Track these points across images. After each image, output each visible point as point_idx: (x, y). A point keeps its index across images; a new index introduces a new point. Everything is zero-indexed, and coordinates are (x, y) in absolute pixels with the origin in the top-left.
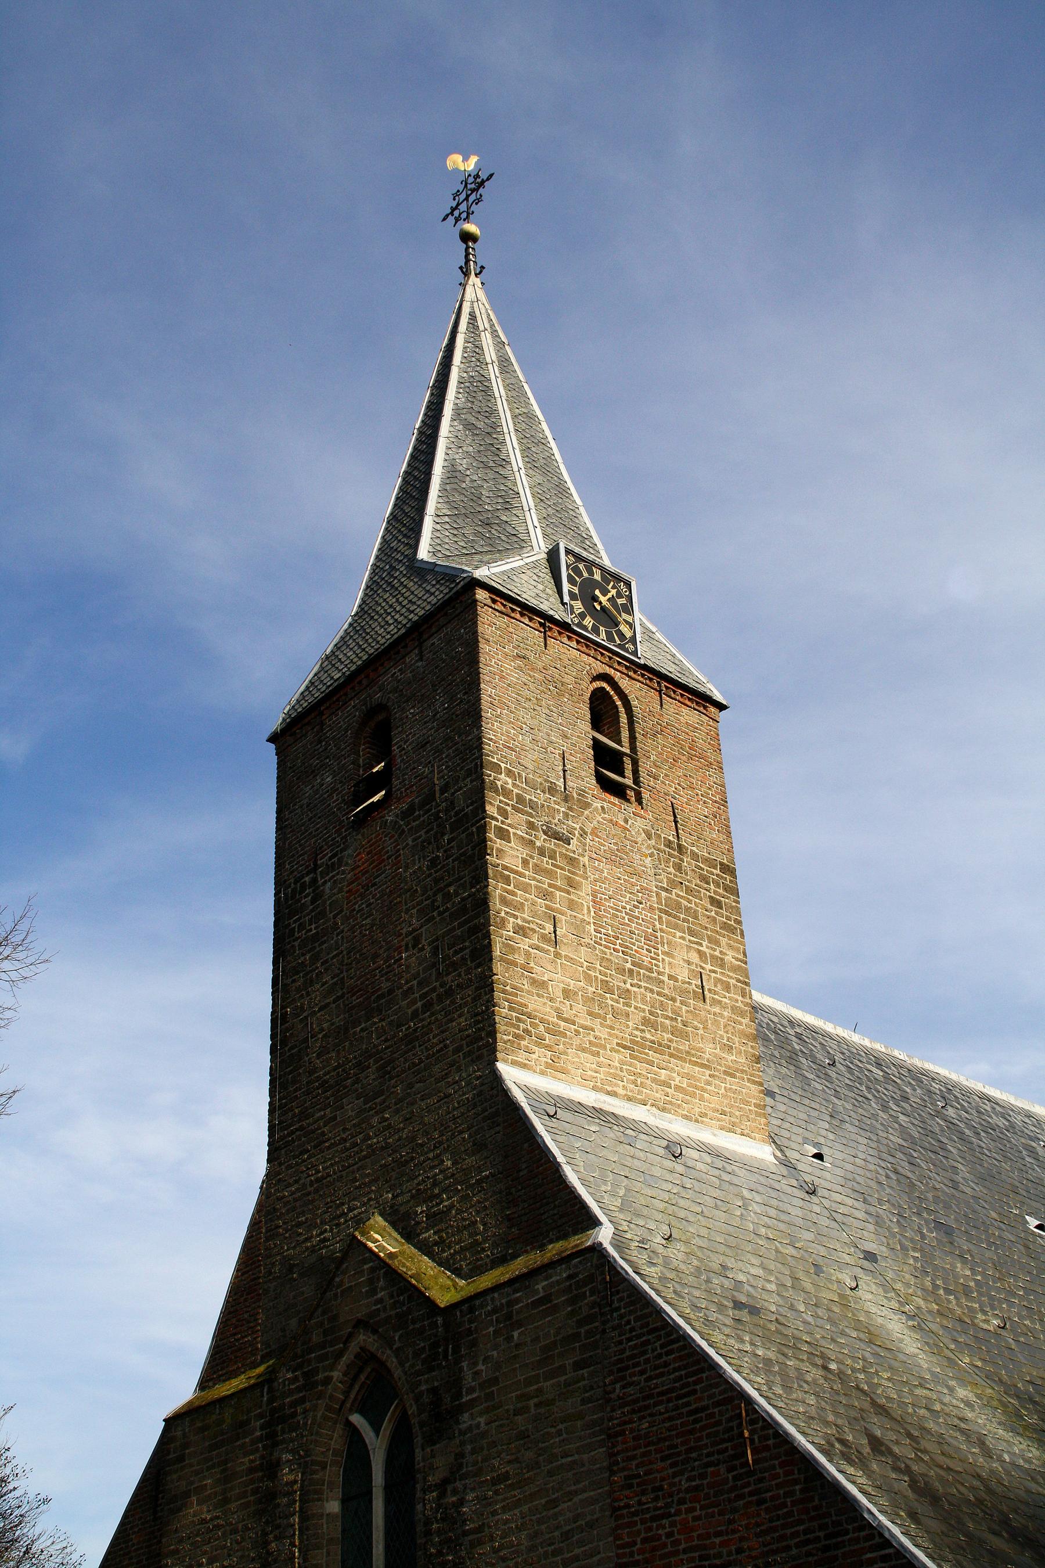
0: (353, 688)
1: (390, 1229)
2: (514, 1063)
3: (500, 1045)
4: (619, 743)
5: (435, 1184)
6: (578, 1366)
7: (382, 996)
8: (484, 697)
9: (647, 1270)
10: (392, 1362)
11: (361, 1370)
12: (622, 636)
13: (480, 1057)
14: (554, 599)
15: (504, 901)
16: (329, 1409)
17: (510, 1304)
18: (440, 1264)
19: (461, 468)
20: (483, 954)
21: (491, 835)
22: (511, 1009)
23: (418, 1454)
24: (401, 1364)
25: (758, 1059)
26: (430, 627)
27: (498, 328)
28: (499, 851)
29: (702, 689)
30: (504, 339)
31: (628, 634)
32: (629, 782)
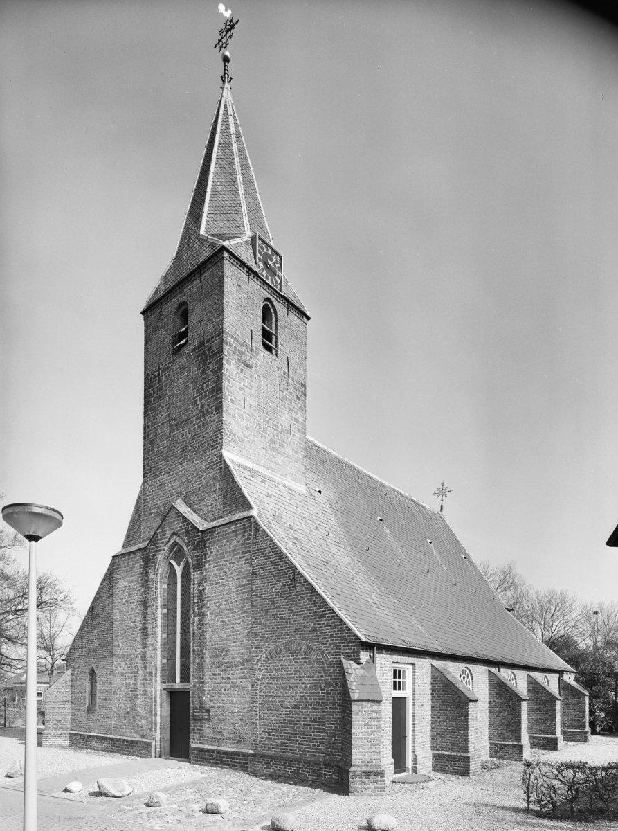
0: (174, 294)
4: (271, 329)
6: (243, 553)
10: (184, 546)
12: (276, 282)
19: (218, 190)
25: (305, 457)
26: (205, 268)
27: (236, 115)
28: (227, 369)
29: (303, 309)
30: (239, 124)
31: (279, 281)
32: (273, 346)
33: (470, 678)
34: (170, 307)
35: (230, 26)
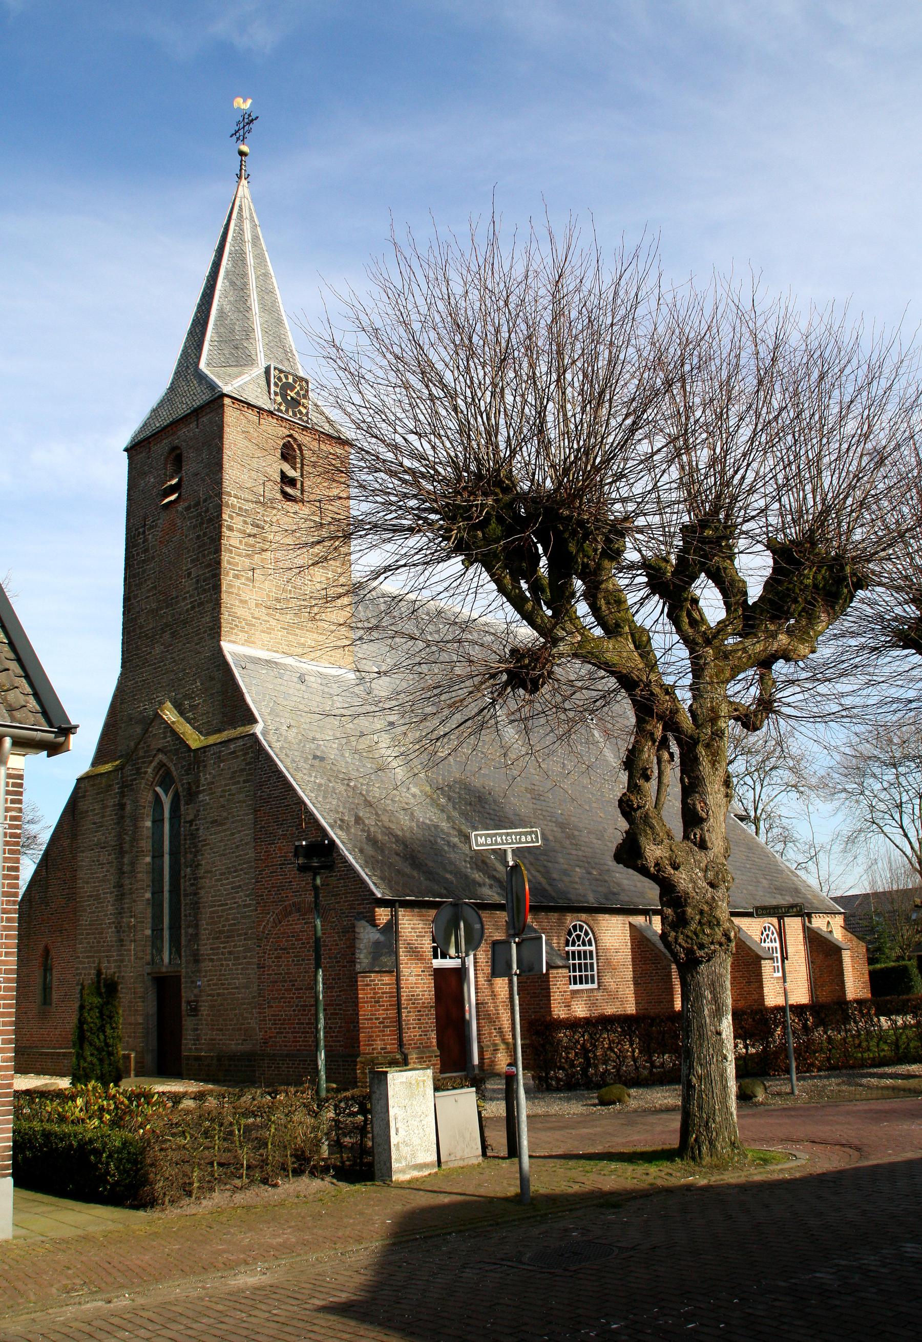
1: (173, 709)
2: (230, 641)
3: (223, 633)
5: (193, 692)
6: (245, 782)
7: (173, 598)
8: (225, 457)
9: (275, 745)
10: (173, 768)
11: (160, 769)
12: (301, 413)
13: (214, 638)
14: (266, 397)
15: (229, 563)
16: (146, 784)
17: (220, 752)
18: (194, 728)
20: (217, 588)
21: (224, 529)
22: (229, 615)
23: (182, 808)
24: (176, 770)
27: (254, 215)
30: (257, 223)
31: (304, 411)
33: (591, 935)
34: (161, 449)
35: (248, 120)
